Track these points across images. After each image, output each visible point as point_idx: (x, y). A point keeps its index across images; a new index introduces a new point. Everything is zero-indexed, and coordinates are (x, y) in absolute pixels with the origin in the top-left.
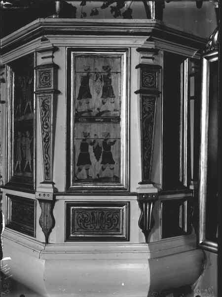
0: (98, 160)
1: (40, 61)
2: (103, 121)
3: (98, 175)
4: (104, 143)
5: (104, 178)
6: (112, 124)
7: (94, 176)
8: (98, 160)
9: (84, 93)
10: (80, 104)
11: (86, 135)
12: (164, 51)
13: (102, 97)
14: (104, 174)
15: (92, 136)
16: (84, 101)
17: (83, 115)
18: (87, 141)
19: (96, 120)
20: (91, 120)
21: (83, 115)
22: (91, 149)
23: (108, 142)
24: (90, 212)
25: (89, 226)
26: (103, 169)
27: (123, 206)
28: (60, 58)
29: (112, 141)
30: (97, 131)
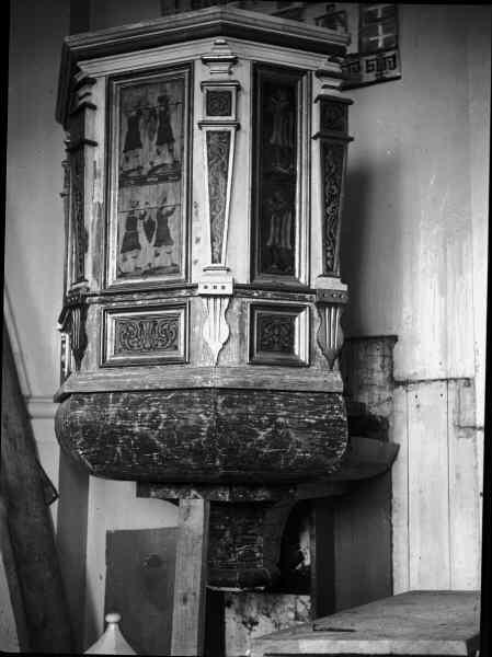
0: (150, 241)
1: (202, 74)
2: (264, 591)
3: (150, 265)
4: (160, 216)
5: (158, 268)
6: (170, 184)
7: (144, 267)
8: (150, 241)
9: (132, 143)
10: (125, 260)
11: (134, 204)
12: (257, 67)
13: (157, 144)
14: (157, 262)
15: (142, 206)
16: (129, 255)
17: (131, 175)
18: (137, 215)
19: (149, 180)
20: (142, 181)
21: (131, 175)
22: (140, 227)
23: (164, 212)
24: (137, 323)
25: (136, 345)
26: (157, 255)
27: (223, 477)
28: (243, 75)
29: (169, 209)
30: (147, 197)
